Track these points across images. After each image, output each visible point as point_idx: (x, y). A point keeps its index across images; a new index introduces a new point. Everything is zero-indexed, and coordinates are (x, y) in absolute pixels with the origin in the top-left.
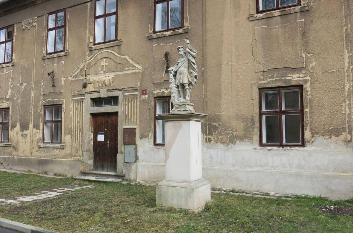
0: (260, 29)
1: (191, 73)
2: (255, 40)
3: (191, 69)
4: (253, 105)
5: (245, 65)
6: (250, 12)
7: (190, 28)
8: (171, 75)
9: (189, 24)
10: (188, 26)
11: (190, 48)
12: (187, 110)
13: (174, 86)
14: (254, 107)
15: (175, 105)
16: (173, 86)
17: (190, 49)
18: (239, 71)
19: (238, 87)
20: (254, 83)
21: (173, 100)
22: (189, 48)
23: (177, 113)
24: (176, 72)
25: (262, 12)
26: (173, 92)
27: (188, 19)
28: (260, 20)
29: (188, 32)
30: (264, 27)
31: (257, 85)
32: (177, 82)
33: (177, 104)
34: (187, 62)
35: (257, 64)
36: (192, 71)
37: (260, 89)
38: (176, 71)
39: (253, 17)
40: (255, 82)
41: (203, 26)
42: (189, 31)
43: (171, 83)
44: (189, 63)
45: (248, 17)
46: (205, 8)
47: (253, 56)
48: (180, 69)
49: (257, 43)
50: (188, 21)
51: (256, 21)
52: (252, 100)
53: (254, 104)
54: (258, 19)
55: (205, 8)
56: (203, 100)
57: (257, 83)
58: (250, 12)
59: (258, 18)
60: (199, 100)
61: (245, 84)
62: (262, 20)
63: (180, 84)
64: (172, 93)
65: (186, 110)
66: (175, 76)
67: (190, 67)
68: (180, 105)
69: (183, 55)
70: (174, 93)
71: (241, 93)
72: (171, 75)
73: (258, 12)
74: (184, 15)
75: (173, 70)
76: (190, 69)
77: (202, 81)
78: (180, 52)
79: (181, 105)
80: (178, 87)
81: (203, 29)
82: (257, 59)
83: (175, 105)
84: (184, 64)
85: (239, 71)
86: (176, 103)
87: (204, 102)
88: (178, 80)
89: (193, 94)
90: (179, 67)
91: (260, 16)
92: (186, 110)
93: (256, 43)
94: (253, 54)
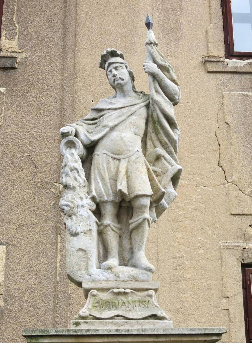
0: (240, 98)
1: (158, 158)
2: (225, 125)
3: (157, 143)
4: (229, 314)
5: (199, 190)
6: (208, 50)
7: (21, 57)
8: (72, 154)
9: (20, 46)
10: (13, 49)
11: (160, 62)
12: (162, 315)
13: (88, 203)
14: (230, 320)
15: (95, 292)
16: (81, 203)
17: (160, 66)
18: (178, 207)
19: (178, 255)
20: (228, 248)
21: (76, 268)
23: (108, 327)
24: (91, 148)
25: (242, 56)
26: (79, 230)
27: (17, 31)
28: (236, 76)
29: (13, 68)
31: (239, 254)
32: (101, 188)
33: (105, 285)
34: (143, 112)
35: (236, 192)
36: (161, 151)
38: (92, 142)
39: (220, 64)
40: (231, 242)
41: (64, 60)
42: (17, 66)
44: (150, 120)
45: (205, 62)
49: (232, 133)
50: (17, 37)
51: (226, 77)
52: (225, 300)
53: (231, 311)
54: (230, 70)
57: (239, 246)
58: (208, 50)
60: (39, 288)
61: (199, 248)
62: (243, 76)
63: (111, 198)
64: (76, 234)
65: (154, 317)
66: (87, 160)
67: (153, 135)
68: (119, 293)
70: (81, 236)
71: (190, 276)
72: (72, 154)
73: (230, 53)
74: (4, 19)
75: (82, 137)
76: (149, 144)
77: (52, 224)
78: (116, 68)
79: (125, 293)
80: (98, 213)
81: (63, 69)
82: (234, 177)
83: (95, 292)
84: (133, 117)
85: (179, 205)
86: (94, 281)
87: (59, 295)
88: (103, 179)
90: (112, 129)
92: (154, 317)
93: (229, 132)
94: (221, 162)
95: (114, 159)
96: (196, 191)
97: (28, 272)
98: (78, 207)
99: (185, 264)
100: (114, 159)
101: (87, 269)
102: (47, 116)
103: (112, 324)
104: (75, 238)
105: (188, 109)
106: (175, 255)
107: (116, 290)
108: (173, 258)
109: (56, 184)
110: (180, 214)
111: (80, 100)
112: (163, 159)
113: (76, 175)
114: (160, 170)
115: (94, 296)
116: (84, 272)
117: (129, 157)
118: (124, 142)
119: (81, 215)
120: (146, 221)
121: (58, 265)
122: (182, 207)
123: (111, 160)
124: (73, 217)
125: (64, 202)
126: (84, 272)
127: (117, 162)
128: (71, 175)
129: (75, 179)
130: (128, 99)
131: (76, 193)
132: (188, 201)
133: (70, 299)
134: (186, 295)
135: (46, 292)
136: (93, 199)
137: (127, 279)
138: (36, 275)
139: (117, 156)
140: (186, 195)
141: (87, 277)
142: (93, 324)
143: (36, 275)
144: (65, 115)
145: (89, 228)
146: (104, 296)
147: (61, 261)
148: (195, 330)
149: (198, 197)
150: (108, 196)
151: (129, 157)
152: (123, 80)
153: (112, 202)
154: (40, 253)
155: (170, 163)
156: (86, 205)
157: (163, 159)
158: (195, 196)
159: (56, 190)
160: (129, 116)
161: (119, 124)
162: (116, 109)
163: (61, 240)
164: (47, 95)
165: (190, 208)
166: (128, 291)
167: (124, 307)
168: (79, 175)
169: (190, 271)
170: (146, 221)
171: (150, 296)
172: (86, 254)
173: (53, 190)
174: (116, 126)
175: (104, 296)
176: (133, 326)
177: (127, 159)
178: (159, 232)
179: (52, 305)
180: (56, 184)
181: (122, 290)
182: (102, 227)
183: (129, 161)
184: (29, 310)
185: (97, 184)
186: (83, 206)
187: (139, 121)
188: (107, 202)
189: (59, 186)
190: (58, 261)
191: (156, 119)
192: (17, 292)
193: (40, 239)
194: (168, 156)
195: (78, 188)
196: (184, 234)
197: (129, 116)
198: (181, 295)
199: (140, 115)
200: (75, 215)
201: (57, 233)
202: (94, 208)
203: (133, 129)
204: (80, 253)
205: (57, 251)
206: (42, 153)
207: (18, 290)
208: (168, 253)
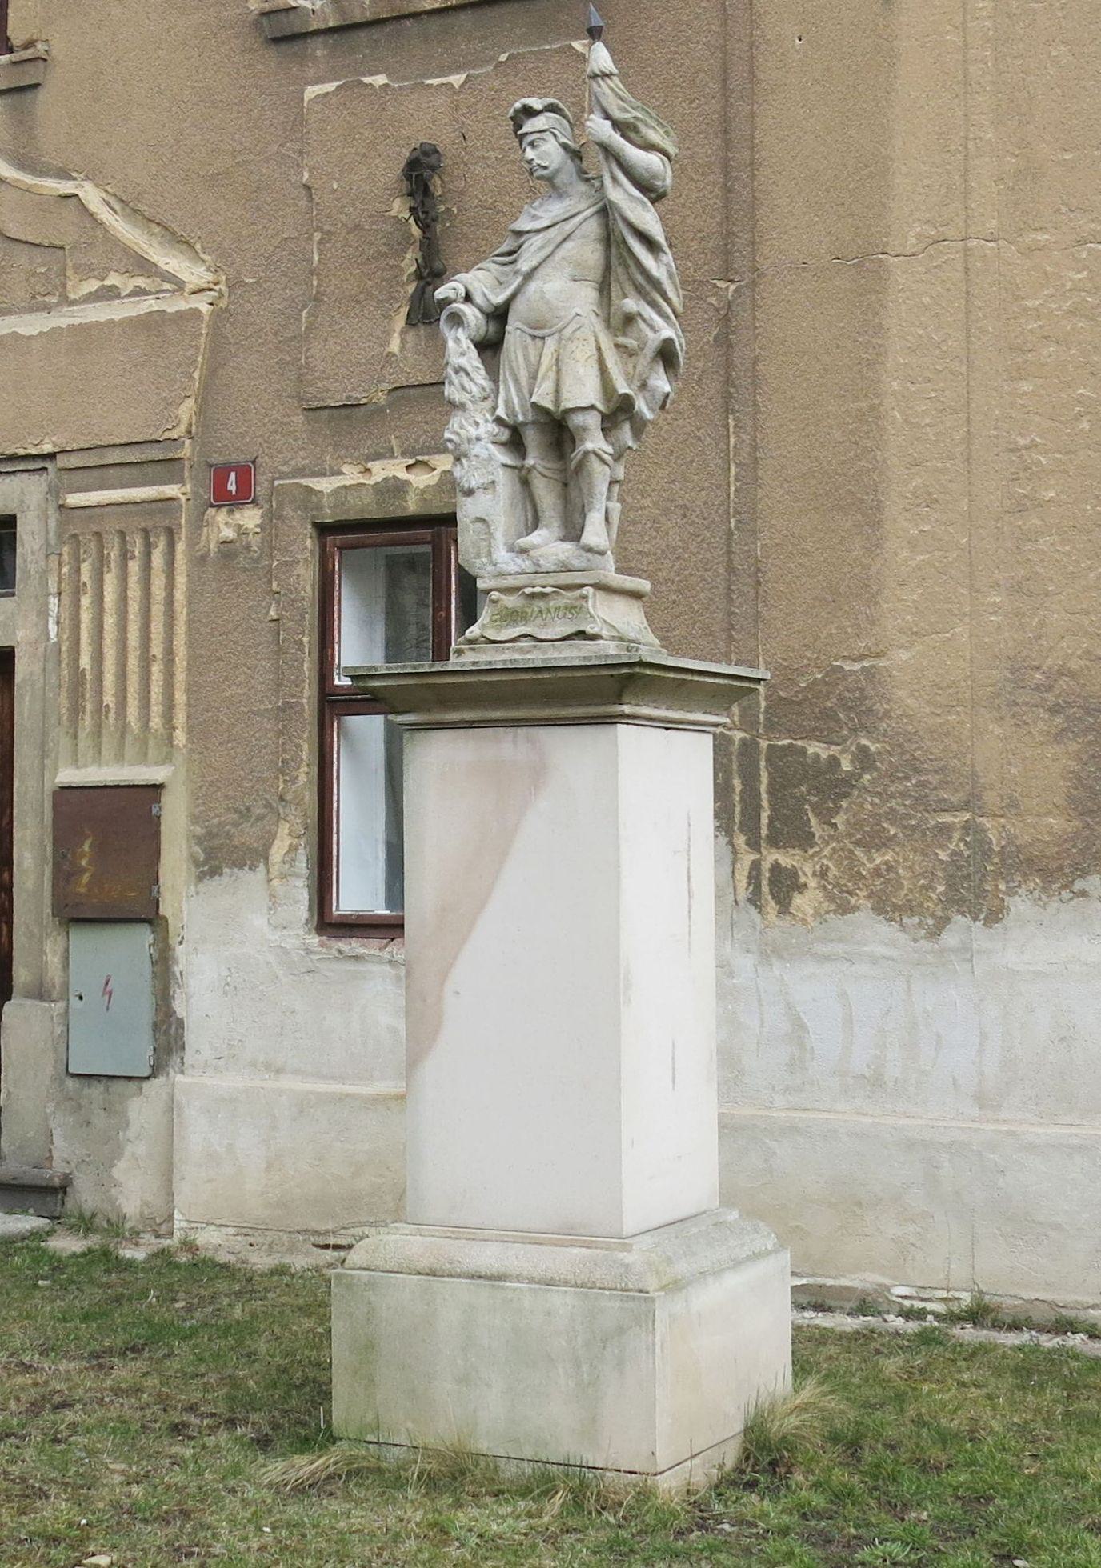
1: (629, 319)
3: (629, 288)
8: (457, 340)
11: (617, 114)
13: (487, 428)
17: (617, 125)
18: (1025, 309)
19: (1022, 442)
21: (472, 551)
23: (507, 656)
26: (474, 484)
32: (511, 401)
33: (510, 582)
34: (593, 227)
36: (632, 304)
38: (497, 308)
43: (462, 407)
44: (610, 240)
48: (533, 286)
56: (729, 552)
60: (693, 547)
61: (1078, 417)
63: (530, 418)
64: (470, 492)
65: (581, 635)
66: (490, 347)
67: (620, 270)
68: (533, 596)
71: (1052, 494)
75: (479, 299)
76: (615, 290)
78: (532, 144)
79: (544, 595)
80: (515, 442)
83: (495, 595)
84: (568, 245)
85: (1029, 303)
86: (501, 575)
88: (517, 381)
89: (647, 502)
90: (529, 276)
92: (581, 635)
95: (534, 337)
96: (1075, 259)
97: (666, 512)
98: (469, 440)
99: (1039, 464)
100: (534, 337)
101: (489, 554)
102: (692, 101)
103: (513, 649)
104: (469, 499)
105: (1059, 14)
106: (1016, 443)
107: (528, 591)
108: (1012, 450)
109: (719, 284)
110: (1031, 331)
111: (767, 42)
112: (640, 321)
113: (465, 380)
114: (635, 343)
115: (495, 602)
116: (485, 560)
117: (560, 331)
118: (548, 302)
119: (477, 456)
120: (593, 457)
121: (732, 488)
122: (1036, 309)
123: (529, 340)
124: (464, 460)
125: (447, 435)
126: (485, 560)
127: (539, 342)
128: (456, 382)
129: (463, 388)
130: (567, 202)
131: (467, 415)
132: (1052, 290)
133: (759, 570)
134: (1041, 544)
135: (709, 556)
136: (499, 421)
137: (553, 568)
138: (685, 516)
139: (538, 331)
140: (1046, 273)
141: (490, 568)
142: (484, 651)
143: (685, 516)
144: (732, 91)
145: (491, 478)
146: (511, 601)
147: (737, 480)
148: (590, 658)
149: (1080, 276)
150: (524, 414)
151: (560, 331)
152: (545, 168)
153: (533, 423)
154: (692, 461)
155: (651, 327)
156: (483, 436)
157: (640, 321)
158: (1071, 274)
159: (720, 298)
160: (558, 246)
161: (540, 264)
162: (539, 231)
163: (736, 426)
164: (688, 40)
165: (1060, 308)
166: (548, 590)
167: (539, 621)
168: (472, 380)
169: (1052, 482)
170: (593, 457)
171: (585, 597)
172: (488, 526)
173: (713, 300)
174: (534, 269)
175: (511, 601)
176: (545, 652)
177: (556, 336)
178: (972, 383)
179: (722, 585)
180: (719, 284)
181: (538, 589)
182: (524, 472)
183: (560, 339)
184: (674, 602)
185: (508, 390)
186: (478, 439)
187: (587, 250)
188: (524, 424)
189: (727, 288)
190: (732, 479)
191: (619, 239)
192: (646, 560)
193: (687, 430)
194: (648, 312)
195: (469, 405)
196: (1039, 382)
197: (558, 246)
198: (1028, 547)
199: (583, 236)
200: (466, 456)
201: (727, 410)
202: (505, 434)
203: (569, 270)
204: (479, 525)
205: (728, 455)
206: (683, 205)
207: (648, 555)
208: (996, 437)
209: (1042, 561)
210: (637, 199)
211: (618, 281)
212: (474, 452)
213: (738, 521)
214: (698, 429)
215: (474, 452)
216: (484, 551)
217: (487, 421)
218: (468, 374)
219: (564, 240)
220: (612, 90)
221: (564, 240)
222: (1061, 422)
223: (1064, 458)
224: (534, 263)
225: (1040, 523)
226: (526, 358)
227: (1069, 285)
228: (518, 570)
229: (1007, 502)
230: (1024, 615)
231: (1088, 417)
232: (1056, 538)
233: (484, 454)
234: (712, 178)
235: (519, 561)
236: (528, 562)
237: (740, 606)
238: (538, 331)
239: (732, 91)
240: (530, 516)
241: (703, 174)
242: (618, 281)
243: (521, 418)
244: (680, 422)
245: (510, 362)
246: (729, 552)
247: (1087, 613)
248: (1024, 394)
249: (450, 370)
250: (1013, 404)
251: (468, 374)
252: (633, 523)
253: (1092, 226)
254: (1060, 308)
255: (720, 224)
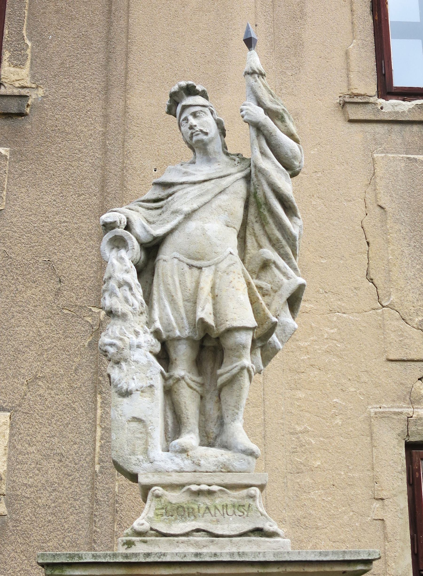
0: (403, 165)
1: (265, 265)
3: (264, 241)
4: (385, 527)
5: (335, 319)
6: (349, 84)
7: (35, 96)
9: (33, 77)
12: (272, 529)
13: (147, 340)
14: (386, 538)
17: (268, 111)
18: (299, 347)
19: (299, 428)
20: (382, 416)
21: (127, 449)
22: (260, 103)
26: (133, 386)
27: (28, 52)
28: (397, 128)
29: (22, 114)
30: (416, 156)
31: (401, 427)
32: (169, 316)
33: (175, 479)
34: (241, 188)
35: (396, 323)
36: (269, 253)
37: (410, 447)
38: (155, 238)
39: (369, 107)
41: (107, 100)
42: (28, 110)
43: (123, 317)
45: (344, 104)
46: (123, 23)
47: (371, 280)
48: (192, 225)
49: (390, 223)
50: (28, 63)
51: (379, 129)
52: (377, 504)
53: (387, 522)
54: (386, 118)
55: (123, 23)
56: (93, 488)
57: (401, 413)
58: (349, 84)
59: (390, 113)
60: (66, 483)
62: (408, 128)
63: (187, 333)
64: (127, 394)
65: (259, 532)
67: (257, 227)
68: (199, 493)
69: (211, 140)
70: (136, 396)
71: (318, 463)
72: (121, 259)
74: (6, 32)
75: (138, 229)
76: (250, 241)
78: (194, 115)
79: (210, 493)
80: (164, 357)
81: (106, 116)
82: (393, 298)
83: (159, 490)
84: (223, 197)
85: (302, 344)
86: (157, 471)
87: (100, 495)
89: (32, 449)
90: (188, 216)
91: (397, 109)
92: (259, 532)
93: (384, 221)
94: (372, 271)
95: (191, 266)
96: (329, 321)
97: (47, 457)
98: (131, 347)
99: (310, 443)
100: (191, 266)
101: (146, 451)
102: (80, 195)
103: (188, 543)
104: (125, 400)
106: (294, 429)
107: (194, 488)
109: (94, 309)
111: (134, 168)
114: (269, 286)
116: (141, 457)
117: (216, 264)
118: (209, 239)
119: (137, 362)
120: (245, 372)
121: (98, 444)
122: (306, 348)
123: (186, 268)
124: (123, 364)
126: (141, 457)
127: (196, 272)
128: (119, 294)
129: (127, 300)
132: (315, 338)
134: (312, 495)
135: (78, 490)
136: (157, 333)
137: (213, 468)
138: (61, 461)
139: (196, 262)
140: (311, 327)
141: (146, 465)
142: (156, 544)
143: (61, 461)
144: (109, 193)
146: (175, 497)
147: (102, 439)
149: (332, 331)
150: (181, 329)
151: (216, 264)
152: (206, 134)
153: (188, 339)
154: (67, 424)
155: (285, 274)
156: (143, 344)
157: (273, 266)
158: (327, 329)
159: (94, 319)
160: (216, 196)
162: (194, 183)
163: (102, 403)
164: (79, 159)
165: (320, 349)
166: (215, 488)
169: (319, 455)
170: (245, 372)
171: (252, 497)
172: (145, 426)
173: (89, 319)
174: (194, 211)
175: (175, 497)
176: (223, 547)
177: (213, 267)
178: (266, 389)
179: (86, 510)
180: (94, 309)
181: (204, 487)
182: (171, 382)
183: (216, 271)
184: (49, 521)
185: (162, 309)
186: (139, 346)
188: (179, 339)
189: (99, 313)
190: (98, 438)
192: (29, 490)
194: (281, 262)
195: (130, 316)
196: (309, 392)
197: (216, 196)
198: (304, 496)
199: (235, 193)
200: (126, 360)
202: (158, 348)
204: (134, 424)
205: (95, 421)
206: (70, 257)
208: (283, 424)
209: (313, 506)
210: (282, 170)
211: (255, 235)
212: (133, 358)
213: (102, 467)
214: (74, 402)
215: (133, 358)
216: (139, 449)
217: (145, 332)
218: (131, 289)
219: (220, 192)
220: (265, 86)
221: (220, 192)
222: (323, 418)
223: (326, 441)
224: (195, 206)
225: (311, 481)
226: (182, 283)
227: (326, 336)
228: (177, 469)
229: (289, 466)
230: (302, 541)
231: (341, 416)
232: (323, 492)
233: (143, 360)
234: (91, 243)
235: (178, 460)
236: (186, 462)
237: (101, 527)
238: (196, 262)
239: (109, 193)
240: (170, 421)
241: (85, 240)
242: (255, 235)
243: (178, 333)
244: (61, 397)
245: (166, 284)
246: (93, 488)
247: (344, 542)
248: (300, 399)
249: (113, 284)
250: (292, 404)
251: (131, 289)
252: (21, 463)
253: (339, 303)
254: (320, 349)
255: (95, 272)
